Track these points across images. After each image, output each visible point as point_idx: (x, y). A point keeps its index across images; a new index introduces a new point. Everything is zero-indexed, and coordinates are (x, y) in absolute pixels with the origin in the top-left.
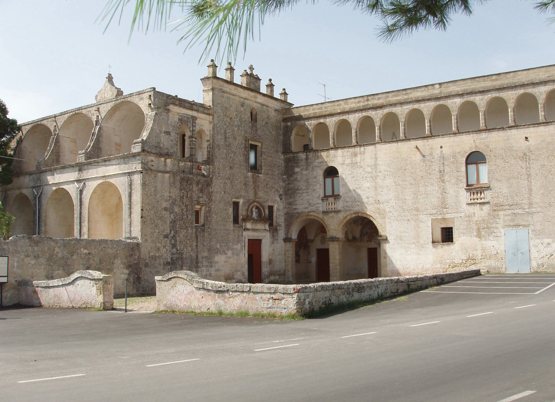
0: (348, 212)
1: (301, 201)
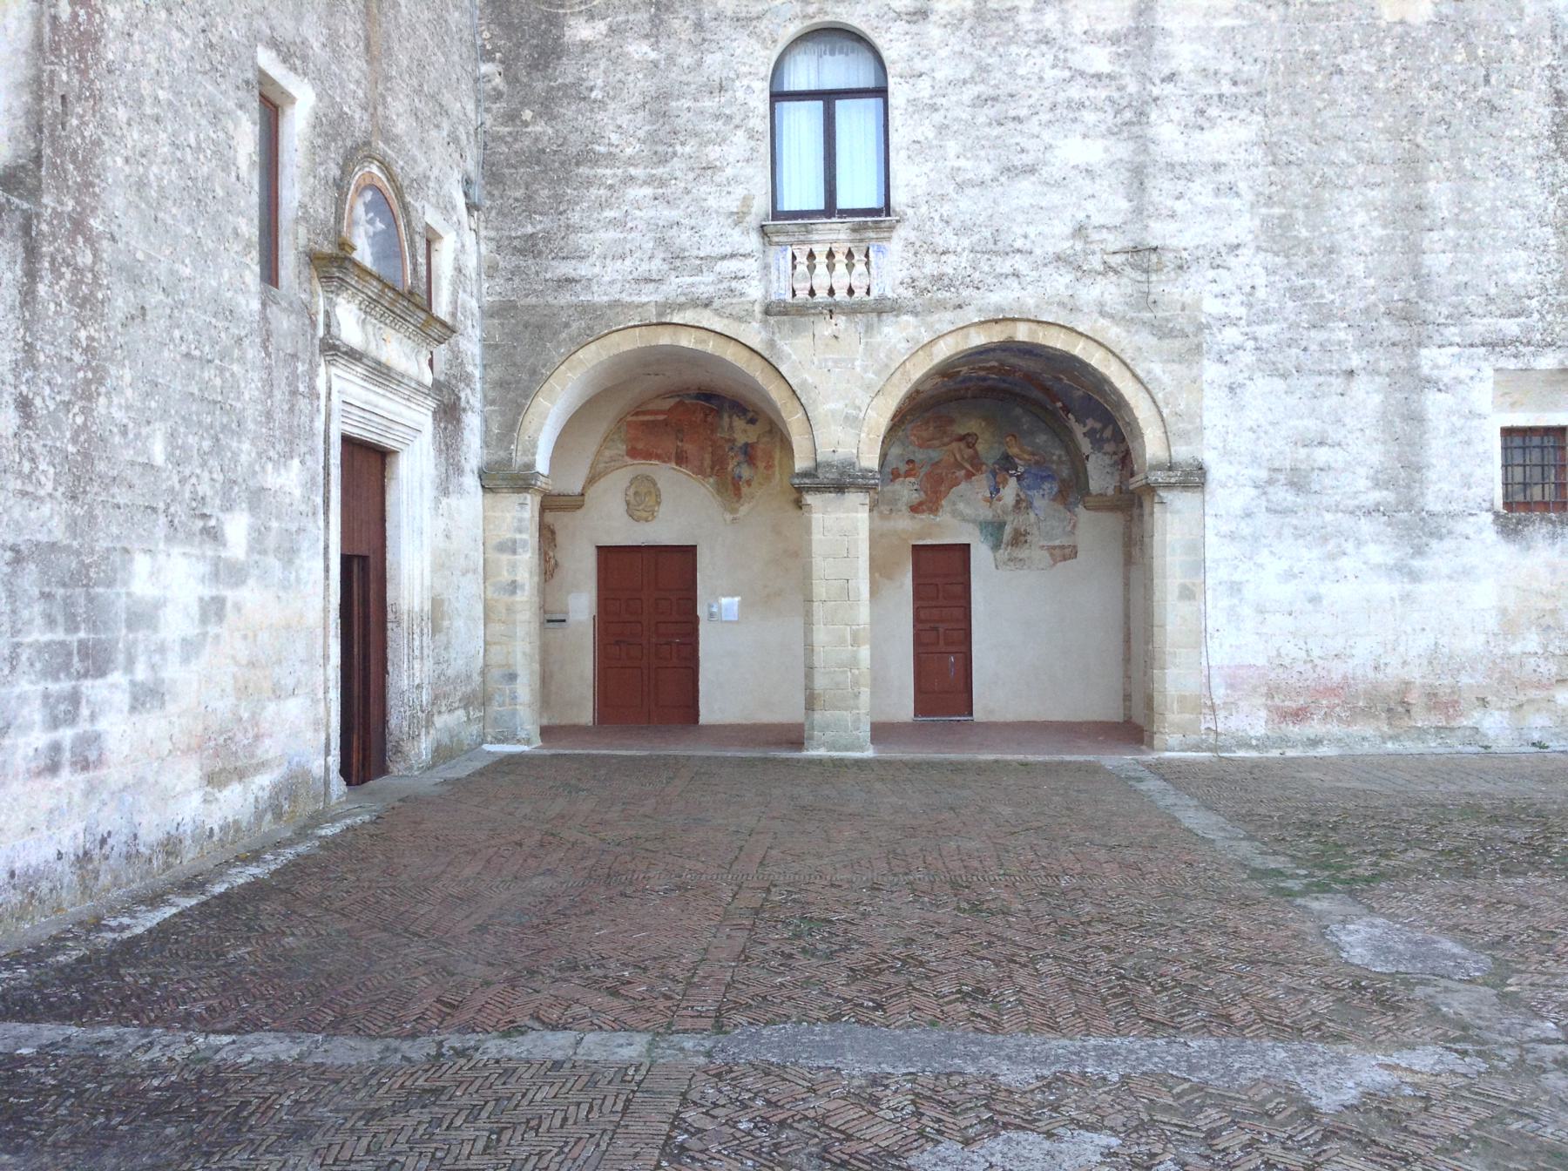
0: (949, 315)
1: (612, 234)
